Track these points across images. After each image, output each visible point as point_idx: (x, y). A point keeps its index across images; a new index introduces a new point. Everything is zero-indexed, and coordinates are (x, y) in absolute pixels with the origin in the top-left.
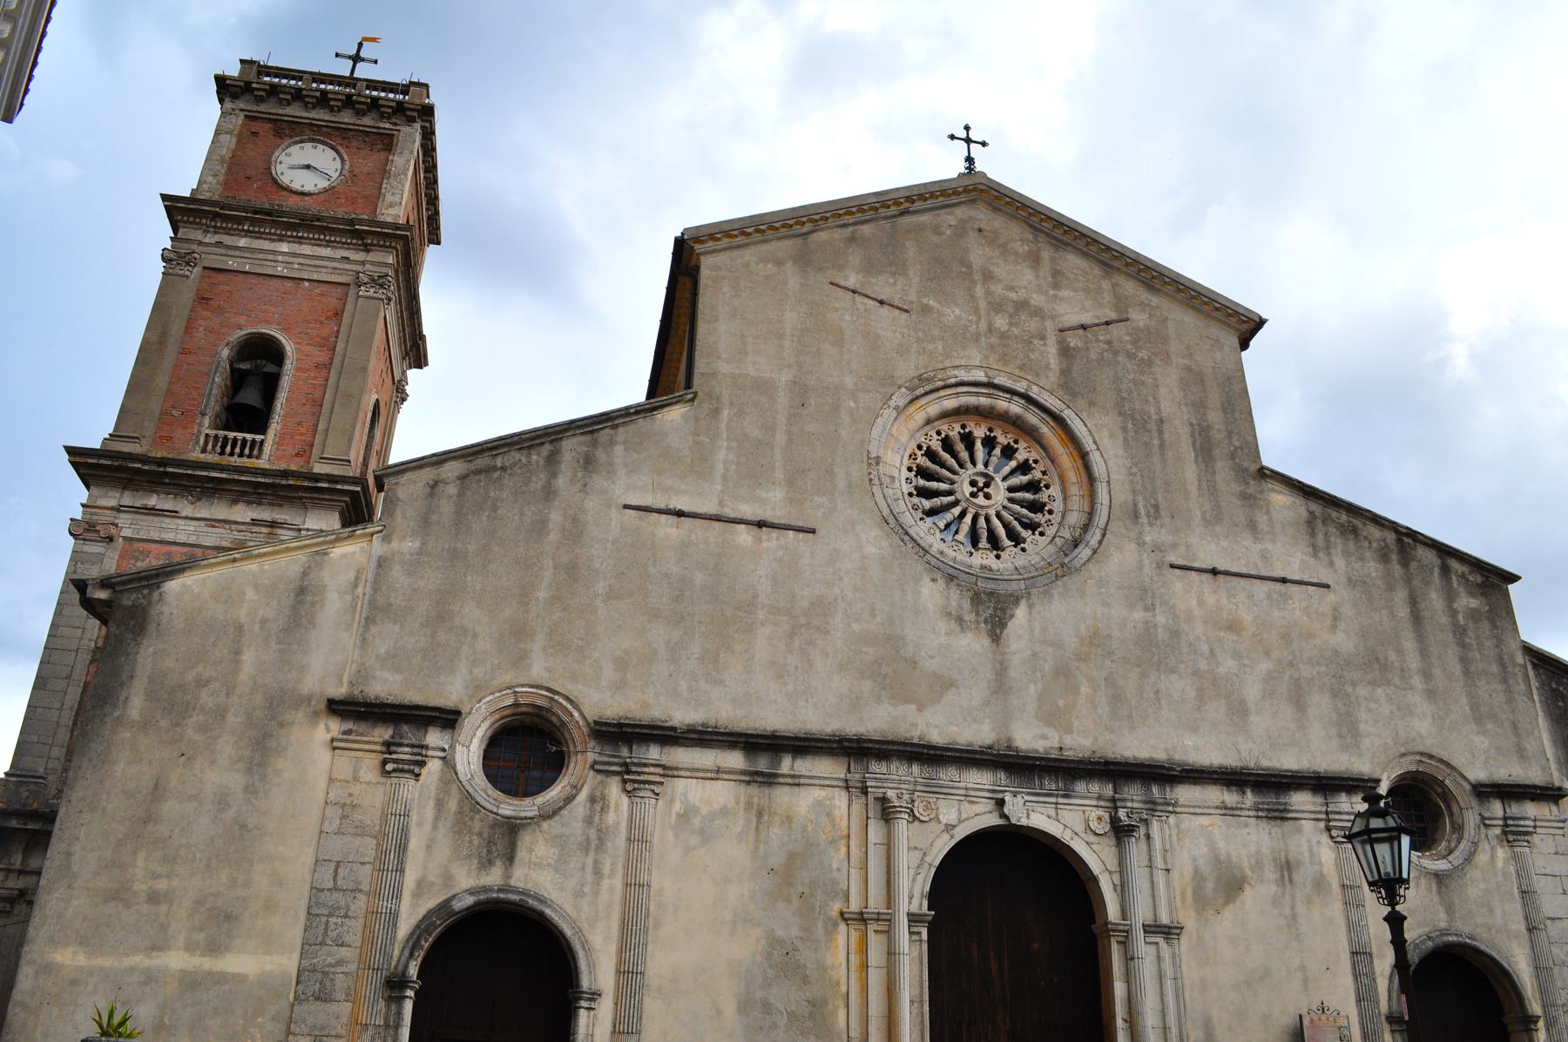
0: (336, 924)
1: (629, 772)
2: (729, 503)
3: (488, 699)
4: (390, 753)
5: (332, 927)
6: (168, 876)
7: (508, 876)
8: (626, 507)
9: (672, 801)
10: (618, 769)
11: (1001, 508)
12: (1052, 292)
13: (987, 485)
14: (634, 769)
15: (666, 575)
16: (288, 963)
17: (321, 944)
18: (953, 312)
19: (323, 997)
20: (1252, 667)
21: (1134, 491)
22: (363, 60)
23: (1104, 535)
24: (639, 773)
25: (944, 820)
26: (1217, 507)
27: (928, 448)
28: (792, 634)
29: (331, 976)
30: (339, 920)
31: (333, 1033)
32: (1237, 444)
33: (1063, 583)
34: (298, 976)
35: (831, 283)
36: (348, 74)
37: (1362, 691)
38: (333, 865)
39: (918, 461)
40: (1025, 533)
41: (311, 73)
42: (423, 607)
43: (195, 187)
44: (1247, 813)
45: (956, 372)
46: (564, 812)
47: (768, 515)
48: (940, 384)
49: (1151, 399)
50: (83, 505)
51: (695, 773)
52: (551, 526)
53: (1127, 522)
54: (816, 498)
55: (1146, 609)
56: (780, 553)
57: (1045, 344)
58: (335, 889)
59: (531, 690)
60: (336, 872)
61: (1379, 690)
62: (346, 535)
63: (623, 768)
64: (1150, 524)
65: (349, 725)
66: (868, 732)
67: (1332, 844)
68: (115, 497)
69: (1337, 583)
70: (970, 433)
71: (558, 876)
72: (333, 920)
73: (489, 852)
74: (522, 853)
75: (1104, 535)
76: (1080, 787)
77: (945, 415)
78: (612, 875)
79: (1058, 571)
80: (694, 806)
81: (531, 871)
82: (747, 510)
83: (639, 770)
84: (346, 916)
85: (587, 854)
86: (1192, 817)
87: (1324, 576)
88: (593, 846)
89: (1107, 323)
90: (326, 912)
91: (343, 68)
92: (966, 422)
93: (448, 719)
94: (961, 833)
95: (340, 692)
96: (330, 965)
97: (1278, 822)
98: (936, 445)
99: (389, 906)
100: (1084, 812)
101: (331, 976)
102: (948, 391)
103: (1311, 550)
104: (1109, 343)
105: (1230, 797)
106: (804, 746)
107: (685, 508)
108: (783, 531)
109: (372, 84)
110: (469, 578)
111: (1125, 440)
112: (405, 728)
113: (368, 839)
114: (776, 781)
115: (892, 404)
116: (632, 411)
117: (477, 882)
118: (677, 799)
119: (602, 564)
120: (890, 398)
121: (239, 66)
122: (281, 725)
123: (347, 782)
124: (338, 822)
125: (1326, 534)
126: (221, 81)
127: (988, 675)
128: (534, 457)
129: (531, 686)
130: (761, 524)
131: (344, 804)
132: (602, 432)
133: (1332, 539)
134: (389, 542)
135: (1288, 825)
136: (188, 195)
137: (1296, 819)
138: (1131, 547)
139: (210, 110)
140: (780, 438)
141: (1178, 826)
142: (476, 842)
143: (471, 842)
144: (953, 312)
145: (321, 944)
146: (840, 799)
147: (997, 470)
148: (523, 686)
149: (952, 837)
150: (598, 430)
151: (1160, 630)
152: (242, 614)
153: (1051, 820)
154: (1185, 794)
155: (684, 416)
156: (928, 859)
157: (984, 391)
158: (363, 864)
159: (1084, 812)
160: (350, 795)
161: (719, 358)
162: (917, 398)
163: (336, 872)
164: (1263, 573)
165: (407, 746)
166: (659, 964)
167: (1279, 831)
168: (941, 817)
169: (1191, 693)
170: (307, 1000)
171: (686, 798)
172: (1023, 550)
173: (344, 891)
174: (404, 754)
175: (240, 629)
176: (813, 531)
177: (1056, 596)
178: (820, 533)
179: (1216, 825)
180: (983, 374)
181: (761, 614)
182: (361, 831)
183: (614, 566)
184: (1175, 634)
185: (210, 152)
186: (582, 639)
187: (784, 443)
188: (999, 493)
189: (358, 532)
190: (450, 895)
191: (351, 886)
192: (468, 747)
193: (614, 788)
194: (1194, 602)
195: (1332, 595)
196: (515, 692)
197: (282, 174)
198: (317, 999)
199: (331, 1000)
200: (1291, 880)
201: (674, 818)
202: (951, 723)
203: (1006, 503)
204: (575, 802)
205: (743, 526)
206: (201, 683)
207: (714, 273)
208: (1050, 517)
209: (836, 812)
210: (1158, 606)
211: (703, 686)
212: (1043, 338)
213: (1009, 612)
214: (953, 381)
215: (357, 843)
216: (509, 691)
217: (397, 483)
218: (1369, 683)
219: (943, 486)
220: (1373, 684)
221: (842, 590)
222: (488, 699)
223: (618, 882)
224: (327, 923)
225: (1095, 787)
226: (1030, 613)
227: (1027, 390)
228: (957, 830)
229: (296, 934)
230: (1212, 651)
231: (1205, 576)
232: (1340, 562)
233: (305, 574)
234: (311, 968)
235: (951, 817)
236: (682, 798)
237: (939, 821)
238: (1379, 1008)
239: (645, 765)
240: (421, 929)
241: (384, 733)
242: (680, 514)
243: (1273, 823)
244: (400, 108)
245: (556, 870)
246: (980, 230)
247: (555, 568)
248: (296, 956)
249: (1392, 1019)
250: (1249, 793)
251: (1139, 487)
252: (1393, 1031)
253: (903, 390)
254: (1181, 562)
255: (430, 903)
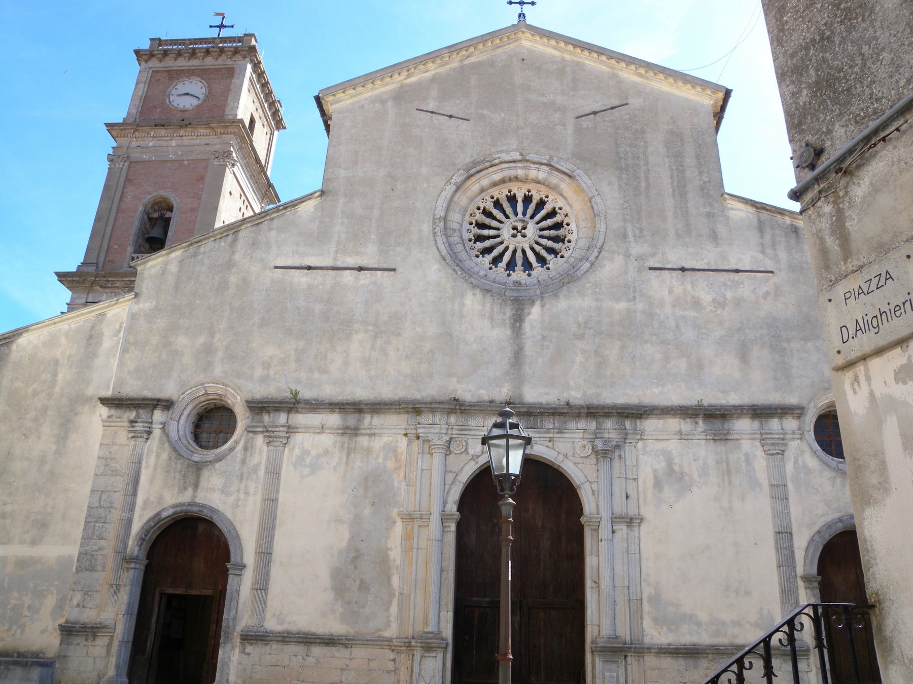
0: (99, 527)
1: (267, 431)
2: (340, 258)
3: (189, 392)
4: (133, 427)
5: (97, 529)
6: (12, 503)
7: (194, 496)
8: (276, 267)
9: (293, 448)
10: (261, 429)
11: (533, 242)
12: (571, 93)
13: (524, 228)
14: (270, 429)
15: (298, 307)
16: (72, 550)
17: (90, 538)
18: (500, 115)
19: (91, 569)
20: (708, 335)
21: (624, 221)
22: (225, 27)
23: (600, 252)
24: (273, 432)
25: (471, 452)
26: (687, 225)
27: (484, 209)
28: (375, 337)
29: (95, 557)
30: (101, 525)
31: (94, 589)
32: (706, 179)
33: (568, 288)
34: (78, 557)
35: (417, 110)
36: (217, 36)
37: (795, 345)
38: (99, 493)
39: (476, 218)
40: (549, 257)
41: (189, 40)
42: (155, 340)
43: (125, 117)
44: (697, 437)
45: (499, 155)
46: (229, 457)
47: (364, 262)
48: (488, 164)
49: (641, 156)
50: (67, 304)
51: (308, 429)
52: (230, 284)
53: (618, 242)
54: (397, 249)
55: (628, 301)
56: (371, 286)
57: (565, 129)
58: (100, 507)
59: (213, 385)
60: (100, 497)
61: (810, 344)
62: (114, 302)
63: (264, 429)
64: (636, 242)
65: (113, 412)
66: (423, 397)
67: (765, 456)
68: (84, 298)
69: (780, 270)
70: (532, 196)
71: (224, 496)
72: (98, 525)
73: (185, 483)
74: (203, 483)
75: (600, 252)
76: (572, 425)
77: (495, 184)
78: (255, 494)
79: (565, 280)
80: (307, 450)
81: (208, 493)
82: (351, 261)
83: (273, 429)
84: (105, 522)
85: (241, 482)
86: (656, 442)
87: (769, 265)
88: (245, 477)
89: (613, 108)
90: (94, 520)
91: (214, 33)
92: (511, 188)
93: (167, 405)
94: (812, 429)
95: (109, 393)
96: (95, 551)
97: (722, 442)
98: (490, 206)
99: (781, 515)
100: (573, 442)
101: (95, 557)
102: (495, 168)
103: (760, 249)
104: (612, 121)
105: (686, 425)
106: (378, 407)
107: (312, 265)
108: (373, 272)
109: (232, 39)
110: (181, 321)
111: (620, 185)
112: (141, 411)
113: (118, 478)
114: (359, 432)
115: (453, 181)
116: (281, 208)
117: (177, 500)
118: (297, 447)
119: (259, 304)
120: (451, 178)
121: (149, 42)
122: (76, 414)
123: (109, 445)
124: (103, 469)
125: (773, 235)
126: (137, 52)
127: (509, 354)
128: (223, 244)
129: (214, 383)
130: (360, 269)
131: (107, 458)
132: (263, 224)
133: (778, 239)
134: (138, 304)
135: (730, 444)
136: (121, 121)
137: (737, 439)
138: (619, 260)
139: (132, 69)
140: (376, 213)
141: (644, 449)
142: (178, 477)
143: (174, 477)
144: (500, 115)
145: (90, 538)
146: (403, 442)
147: (532, 217)
148: (208, 383)
149: (477, 463)
150: (261, 222)
151: (638, 314)
152: (58, 353)
153: (549, 449)
154: (650, 425)
155: (316, 207)
156: (459, 478)
157: (520, 165)
158: (115, 492)
159: (573, 442)
160: (110, 453)
161: (339, 168)
162: (472, 175)
163: (100, 497)
164: (720, 268)
165: (141, 422)
166: (281, 547)
167: (723, 448)
168: (469, 450)
169: (658, 356)
170: (82, 570)
171: (303, 445)
172: (548, 269)
173: (104, 508)
174: (139, 427)
175: (57, 362)
176: (394, 270)
177: (562, 297)
178: (399, 270)
179: (673, 445)
180: (518, 154)
181: (356, 326)
182: (115, 473)
183: (266, 305)
184: (651, 315)
185: (133, 96)
186: (244, 352)
187: (378, 216)
188: (532, 230)
189: (120, 300)
190: (162, 508)
191: (108, 504)
192: (178, 421)
193: (260, 440)
194: (666, 292)
195: (775, 277)
196: (204, 387)
197: (173, 101)
198: (87, 570)
199: (95, 571)
200: (730, 483)
201: (294, 458)
202: (481, 388)
203: (537, 238)
204: (235, 451)
205: (348, 271)
206: (35, 394)
207: (341, 115)
208: (569, 244)
209: (399, 451)
210: (638, 297)
211: (316, 375)
212: (564, 125)
213: (526, 311)
214: (497, 161)
215: (112, 480)
216: (201, 387)
217: (144, 269)
218: (802, 340)
219: (492, 232)
220: (806, 339)
221: (411, 307)
222: (189, 392)
223: (259, 498)
224: (94, 526)
225: (582, 424)
226: (542, 310)
227: (549, 161)
228: (479, 459)
229: (78, 533)
230: (678, 327)
231: (675, 273)
232: (783, 255)
233: (93, 327)
234: (84, 552)
235: (476, 450)
236: (300, 446)
237: (468, 454)
238: (795, 572)
239: (277, 426)
240: (146, 530)
241: (132, 415)
242: (309, 268)
243: (718, 443)
244: (236, 51)
245: (222, 492)
246: (523, 60)
247: (231, 310)
248: (78, 546)
249: (806, 579)
250: (700, 422)
251: (628, 217)
252: (806, 588)
253: (462, 172)
254: (657, 265)
255: (149, 514)
